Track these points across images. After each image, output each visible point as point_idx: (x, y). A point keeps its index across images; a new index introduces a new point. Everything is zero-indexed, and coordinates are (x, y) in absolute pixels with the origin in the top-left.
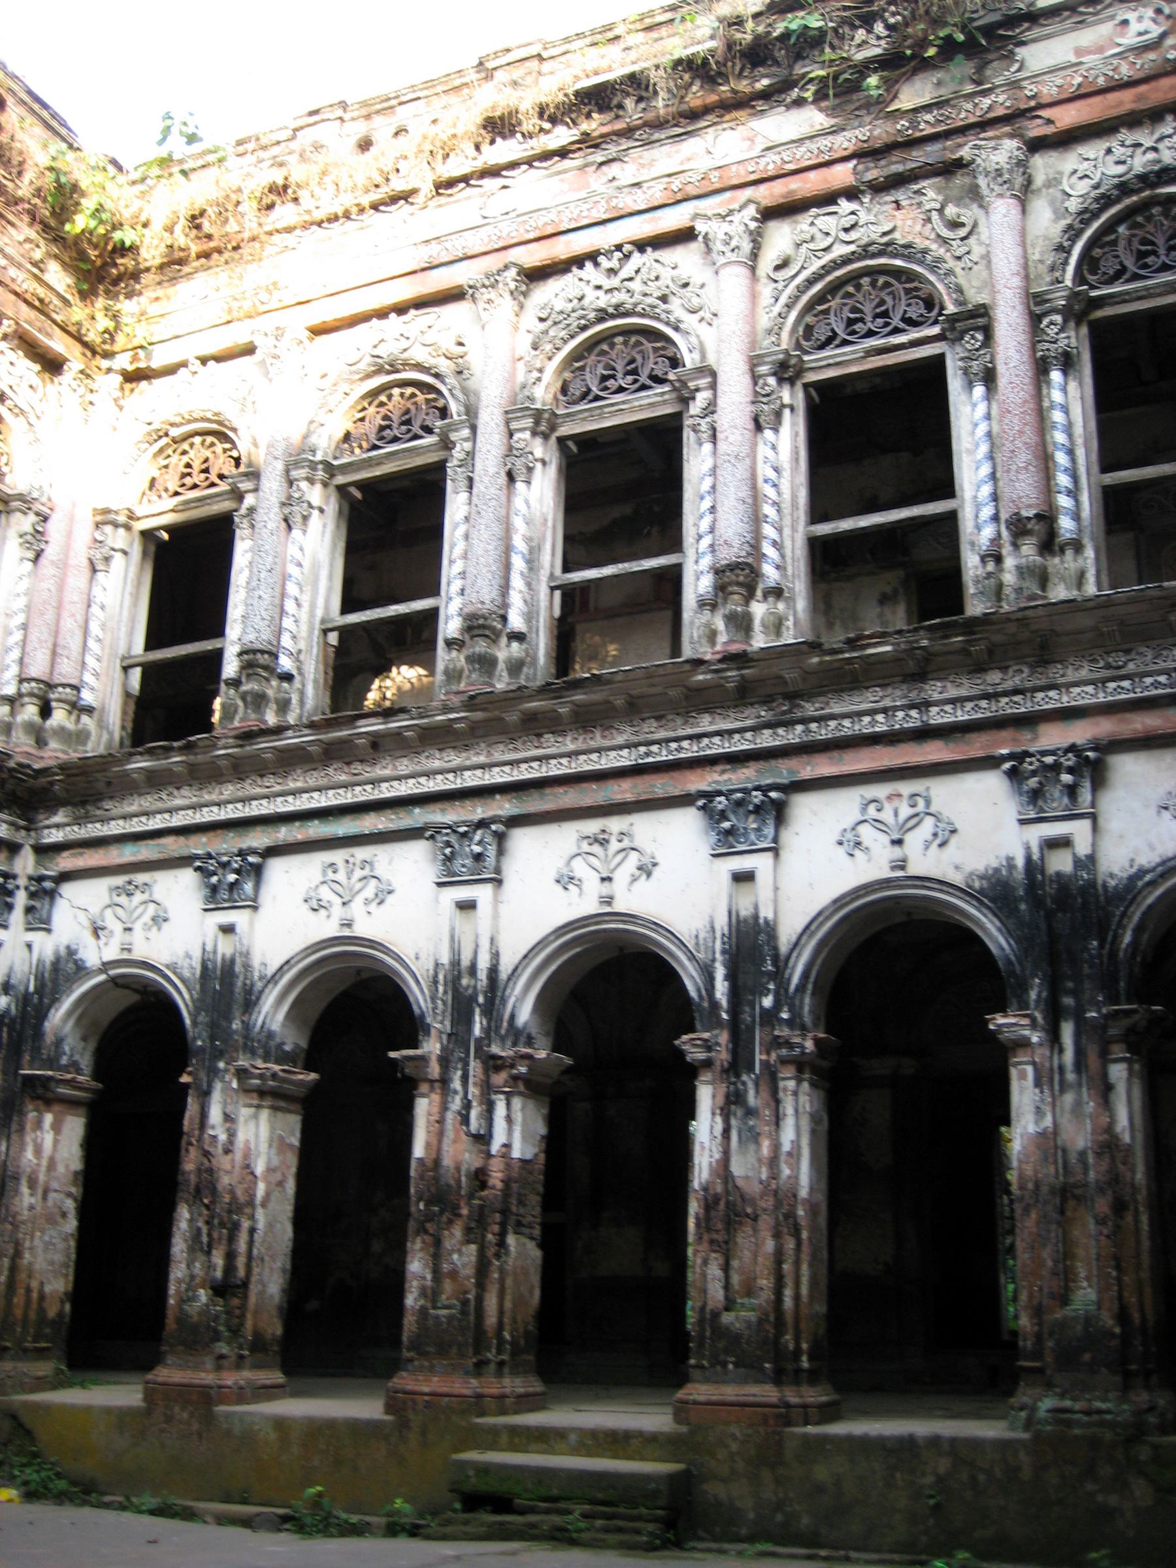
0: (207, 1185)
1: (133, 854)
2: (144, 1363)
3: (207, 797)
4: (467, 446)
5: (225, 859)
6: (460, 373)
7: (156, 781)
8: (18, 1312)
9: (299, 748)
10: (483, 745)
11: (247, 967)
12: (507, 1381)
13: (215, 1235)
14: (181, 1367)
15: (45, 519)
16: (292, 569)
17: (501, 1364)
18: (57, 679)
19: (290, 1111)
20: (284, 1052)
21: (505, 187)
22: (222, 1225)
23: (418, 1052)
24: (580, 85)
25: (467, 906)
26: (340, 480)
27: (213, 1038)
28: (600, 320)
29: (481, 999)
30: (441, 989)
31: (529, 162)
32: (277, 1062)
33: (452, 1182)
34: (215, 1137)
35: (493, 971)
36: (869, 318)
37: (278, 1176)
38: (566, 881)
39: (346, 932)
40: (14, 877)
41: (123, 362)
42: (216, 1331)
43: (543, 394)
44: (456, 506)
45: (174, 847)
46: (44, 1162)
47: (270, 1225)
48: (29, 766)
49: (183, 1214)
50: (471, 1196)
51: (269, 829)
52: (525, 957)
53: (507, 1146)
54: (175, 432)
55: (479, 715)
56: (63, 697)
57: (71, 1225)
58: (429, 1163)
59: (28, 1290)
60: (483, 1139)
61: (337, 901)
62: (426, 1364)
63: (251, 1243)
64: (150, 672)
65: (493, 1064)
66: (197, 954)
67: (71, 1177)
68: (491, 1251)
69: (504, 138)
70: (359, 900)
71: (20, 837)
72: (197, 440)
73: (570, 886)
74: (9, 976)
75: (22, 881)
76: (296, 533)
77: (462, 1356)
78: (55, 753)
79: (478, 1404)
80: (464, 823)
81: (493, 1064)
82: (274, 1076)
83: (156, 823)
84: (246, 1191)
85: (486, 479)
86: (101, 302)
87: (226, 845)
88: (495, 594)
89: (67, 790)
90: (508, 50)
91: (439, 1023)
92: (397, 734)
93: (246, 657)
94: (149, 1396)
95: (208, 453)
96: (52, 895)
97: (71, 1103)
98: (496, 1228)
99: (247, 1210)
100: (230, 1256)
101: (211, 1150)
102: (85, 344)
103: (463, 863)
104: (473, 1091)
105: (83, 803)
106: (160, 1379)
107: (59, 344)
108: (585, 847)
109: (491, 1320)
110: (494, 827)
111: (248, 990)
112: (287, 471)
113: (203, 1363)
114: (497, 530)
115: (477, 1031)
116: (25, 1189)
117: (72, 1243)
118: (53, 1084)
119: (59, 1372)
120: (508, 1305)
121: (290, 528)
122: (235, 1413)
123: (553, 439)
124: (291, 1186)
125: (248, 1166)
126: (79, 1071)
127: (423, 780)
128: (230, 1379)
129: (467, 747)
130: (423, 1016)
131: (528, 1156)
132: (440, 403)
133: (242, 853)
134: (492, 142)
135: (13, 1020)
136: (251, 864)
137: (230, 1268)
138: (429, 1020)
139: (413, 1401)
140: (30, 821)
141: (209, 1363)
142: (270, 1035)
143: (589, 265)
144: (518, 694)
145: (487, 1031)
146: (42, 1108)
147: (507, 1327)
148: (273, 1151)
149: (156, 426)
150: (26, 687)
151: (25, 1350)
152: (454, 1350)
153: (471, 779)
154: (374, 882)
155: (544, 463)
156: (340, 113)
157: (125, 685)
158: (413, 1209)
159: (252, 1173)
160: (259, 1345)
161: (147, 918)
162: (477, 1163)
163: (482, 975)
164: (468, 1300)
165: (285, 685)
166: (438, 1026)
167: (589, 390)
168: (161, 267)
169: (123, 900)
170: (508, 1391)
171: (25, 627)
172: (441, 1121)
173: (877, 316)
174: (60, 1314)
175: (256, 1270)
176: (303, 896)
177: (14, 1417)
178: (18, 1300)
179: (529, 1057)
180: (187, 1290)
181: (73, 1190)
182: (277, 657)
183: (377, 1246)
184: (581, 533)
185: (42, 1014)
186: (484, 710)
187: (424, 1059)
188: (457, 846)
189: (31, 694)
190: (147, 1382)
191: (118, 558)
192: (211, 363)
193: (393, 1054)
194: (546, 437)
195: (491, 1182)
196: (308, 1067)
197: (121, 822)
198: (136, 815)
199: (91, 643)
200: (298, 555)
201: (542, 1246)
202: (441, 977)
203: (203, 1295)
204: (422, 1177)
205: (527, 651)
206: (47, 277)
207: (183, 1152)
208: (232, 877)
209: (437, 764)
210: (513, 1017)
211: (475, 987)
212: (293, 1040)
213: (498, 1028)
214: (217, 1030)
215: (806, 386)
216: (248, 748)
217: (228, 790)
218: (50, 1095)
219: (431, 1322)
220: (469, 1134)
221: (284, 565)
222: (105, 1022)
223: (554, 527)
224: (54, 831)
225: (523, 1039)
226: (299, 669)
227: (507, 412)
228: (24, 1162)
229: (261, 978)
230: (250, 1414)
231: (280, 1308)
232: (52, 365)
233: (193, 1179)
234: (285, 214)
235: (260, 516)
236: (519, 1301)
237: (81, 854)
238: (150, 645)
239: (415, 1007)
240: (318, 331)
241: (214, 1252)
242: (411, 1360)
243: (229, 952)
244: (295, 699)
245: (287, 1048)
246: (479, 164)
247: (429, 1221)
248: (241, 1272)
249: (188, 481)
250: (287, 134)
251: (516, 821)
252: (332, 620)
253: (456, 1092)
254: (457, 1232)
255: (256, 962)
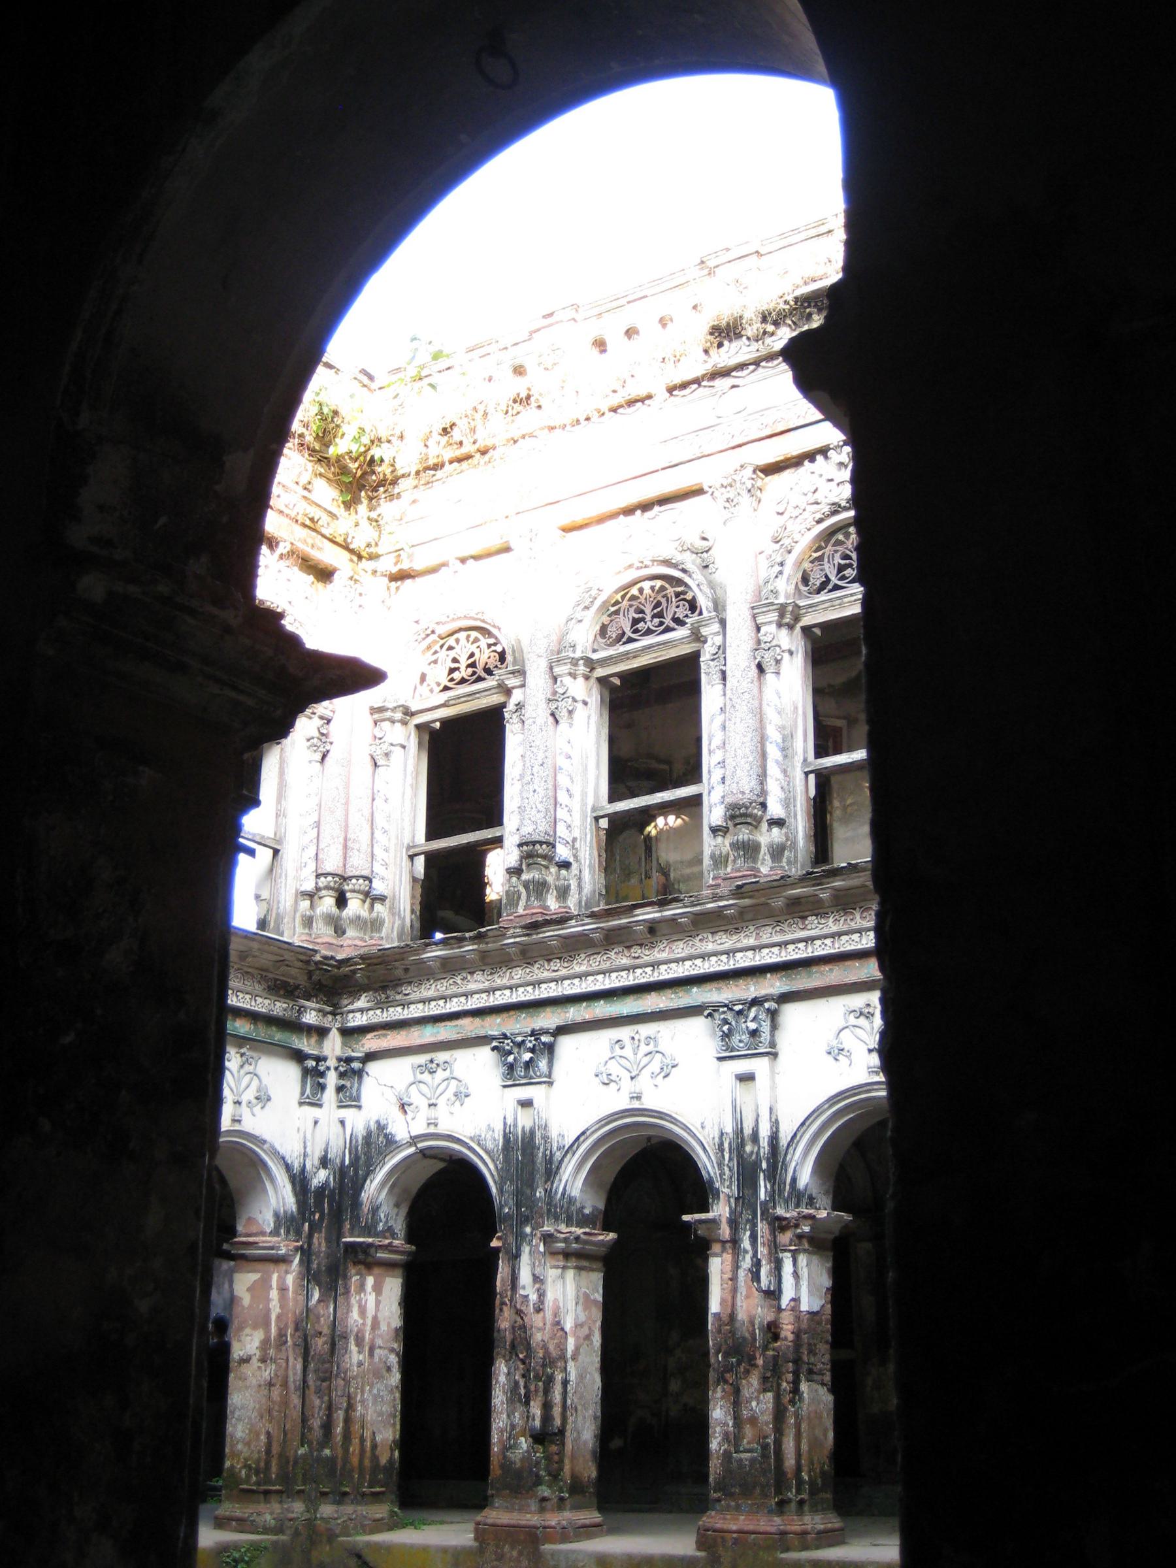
0: (521, 1342)
1: (432, 1035)
2: (480, 1503)
3: (499, 982)
4: (718, 640)
5: (519, 1039)
6: (706, 567)
7: (450, 968)
8: (355, 1460)
9: (581, 935)
10: (752, 928)
11: (546, 1138)
12: (807, 1519)
13: (532, 1388)
14: (510, 1509)
15: (329, 721)
16: (561, 761)
17: (801, 1503)
18: (349, 873)
19: (592, 1270)
20: (583, 1215)
21: (733, 387)
22: (538, 1378)
23: (710, 1215)
24: (798, 293)
25: (747, 1078)
26: (600, 672)
27: (518, 1205)
28: (834, 513)
29: (764, 1165)
30: (727, 1156)
31: (757, 363)
32: (580, 1225)
33: (747, 1335)
34: (527, 1297)
35: (774, 1139)
36: (648, 618)
37: (585, 1331)
38: (837, 1052)
39: (636, 1105)
40: (325, 1059)
41: (387, 565)
42: (537, 1476)
43: (785, 589)
44: (711, 697)
45: (470, 1028)
46: (369, 1322)
47: (581, 1377)
48: (332, 958)
49: (502, 1372)
50: (765, 1348)
51: (559, 1010)
52: (803, 1124)
53: (796, 1300)
54: (442, 630)
55: (747, 902)
56: (357, 887)
57: (395, 1378)
58: (725, 1318)
59: (362, 1440)
60: (773, 1295)
61: (626, 1076)
62: (733, 1504)
63: (565, 1393)
64: (432, 859)
65: (779, 1225)
66: (499, 1127)
67: (392, 1334)
68: (786, 1398)
69: (730, 341)
70: (646, 1073)
71: (327, 1022)
72: (462, 635)
73: (840, 1057)
74: (326, 1152)
75: (332, 1063)
76: (563, 725)
77: (765, 1495)
78: (352, 944)
79: (782, 1540)
80: (739, 1002)
81: (779, 1225)
82: (577, 1239)
83: (454, 1006)
84: (558, 1346)
85: (738, 674)
86: (363, 508)
87: (519, 1025)
88: (754, 783)
89: (368, 977)
90: (728, 250)
91: (727, 1189)
92: (673, 920)
93: (525, 848)
94: (481, 1534)
95: (473, 648)
96: (359, 1074)
97: (390, 1265)
98: (790, 1377)
99: (560, 1364)
100: (547, 1407)
101: (523, 1308)
102: (352, 551)
103: (740, 1039)
104: (762, 1251)
105: (384, 988)
106: (490, 1521)
107: (328, 555)
108: (852, 1020)
109: (790, 1462)
110: (767, 1005)
111: (549, 1160)
112: (551, 668)
113: (529, 1506)
114: (752, 722)
115: (762, 1195)
116: (353, 1347)
117: (398, 1395)
118: (372, 1250)
119: (392, 1514)
120: (804, 1447)
121: (557, 722)
122: (560, 1552)
123: (798, 629)
124: (597, 1339)
125: (558, 1323)
126: (393, 1235)
127: (698, 962)
128: (553, 1519)
129: (737, 930)
130: (711, 1181)
131: (816, 1308)
132: (689, 596)
133: (533, 1033)
134: (720, 345)
135: (332, 1192)
136: (544, 1044)
137: (547, 1418)
138: (717, 1185)
139: (722, 1538)
140: (336, 1006)
141: (534, 1507)
142: (572, 1201)
143: (819, 458)
144: (784, 882)
145: (772, 1195)
146: (364, 1271)
147: (805, 1469)
148: (580, 1308)
149: (423, 625)
150: (323, 882)
151: (363, 1495)
152: (758, 1491)
153: (744, 960)
154: (659, 1056)
155: (791, 653)
156: (573, 314)
157: (411, 872)
158: (712, 1360)
159: (562, 1329)
160: (576, 1487)
161: (449, 1093)
162: (770, 1317)
163: (764, 1143)
164: (768, 1444)
165: (564, 872)
166: (726, 1190)
167: (624, 634)
168: (418, 473)
169: (426, 1077)
170: (809, 1527)
171: (318, 825)
172: (734, 1279)
173: (654, 616)
174: (391, 1461)
175: (570, 1419)
176: (594, 1071)
177: (359, 1556)
178: (354, 1448)
179: (812, 1217)
180: (509, 1438)
181: (395, 1346)
182: (554, 846)
183: (674, 1386)
184: (830, 686)
185: (359, 1187)
186: (750, 897)
187: (714, 1222)
188: (733, 1023)
189: (327, 888)
190: (478, 1524)
191: (397, 752)
192: (471, 562)
193: (686, 1218)
194: (791, 627)
195: (783, 1334)
196: (607, 1228)
197: (420, 1006)
198: (434, 999)
199: (378, 834)
200: (567, 749)
201: (834, 1389)
202: (726, 1145)
203: (524, 1443)
204: (719, 1331)
205: (786, 835)
206: (313, 496)
207: (497, 1311)
208: (527, 1056)
209: (711, 947)
210: (794, 1180)
211: (758, 1153)
212: (592, 1203)
213: (781, 1191)
214: (522, 1197)
215: (418, 727)
216: (534, 937)
217: (519, 974)
218: (370, 1259)
219: (735, 1464)
220: (759, 1290)
221: (554, 757)
222: (414, 1190)
223: (805, 714)
224: (358, 1015)
225: (805, 1201)
226: (575, 856)
227: (753, 608)
228: (351, 1322)
229: (559, 1149)
230: (574, 1552)
231: (594, 1452)
232: (324, 574)
233: (509, 1336)
234: (529, 418)
235: (528, 712)
236: (815, 1444)
237: (385, 1036)
238: (431, 835)
239: (703, 1172)
240: (567, 530)
241: (532, 1403)
242: (719, 1500)
243: (528, 1125)
244: (573, 884)
245: (587, 1211)
246: (708, 367)
247: (728, 1372)
248: (558, 1422)
249: (457, 676)
250: (526, 336)
251: (786, 998)
252: (602, 808)
253: (746, 1252)
254: (754, 1381)
255: (554, 1133)
